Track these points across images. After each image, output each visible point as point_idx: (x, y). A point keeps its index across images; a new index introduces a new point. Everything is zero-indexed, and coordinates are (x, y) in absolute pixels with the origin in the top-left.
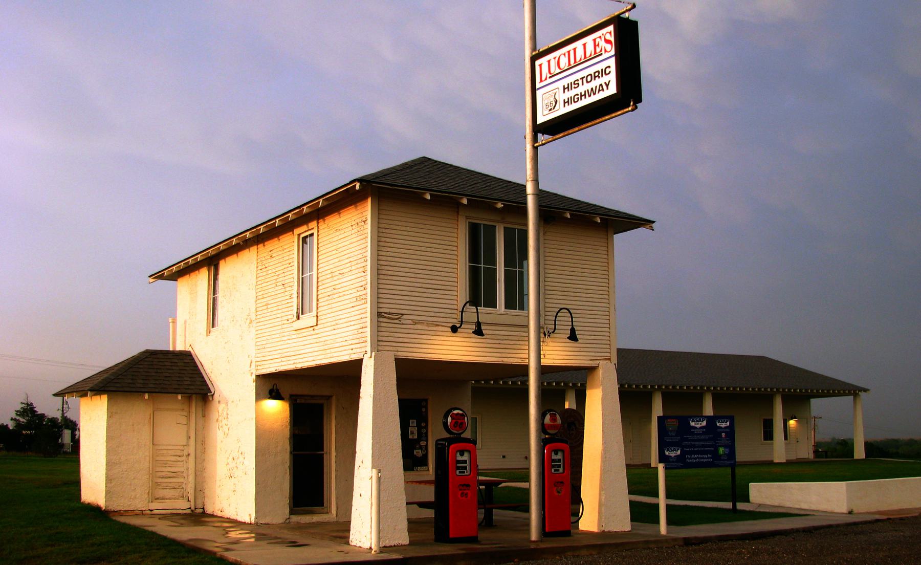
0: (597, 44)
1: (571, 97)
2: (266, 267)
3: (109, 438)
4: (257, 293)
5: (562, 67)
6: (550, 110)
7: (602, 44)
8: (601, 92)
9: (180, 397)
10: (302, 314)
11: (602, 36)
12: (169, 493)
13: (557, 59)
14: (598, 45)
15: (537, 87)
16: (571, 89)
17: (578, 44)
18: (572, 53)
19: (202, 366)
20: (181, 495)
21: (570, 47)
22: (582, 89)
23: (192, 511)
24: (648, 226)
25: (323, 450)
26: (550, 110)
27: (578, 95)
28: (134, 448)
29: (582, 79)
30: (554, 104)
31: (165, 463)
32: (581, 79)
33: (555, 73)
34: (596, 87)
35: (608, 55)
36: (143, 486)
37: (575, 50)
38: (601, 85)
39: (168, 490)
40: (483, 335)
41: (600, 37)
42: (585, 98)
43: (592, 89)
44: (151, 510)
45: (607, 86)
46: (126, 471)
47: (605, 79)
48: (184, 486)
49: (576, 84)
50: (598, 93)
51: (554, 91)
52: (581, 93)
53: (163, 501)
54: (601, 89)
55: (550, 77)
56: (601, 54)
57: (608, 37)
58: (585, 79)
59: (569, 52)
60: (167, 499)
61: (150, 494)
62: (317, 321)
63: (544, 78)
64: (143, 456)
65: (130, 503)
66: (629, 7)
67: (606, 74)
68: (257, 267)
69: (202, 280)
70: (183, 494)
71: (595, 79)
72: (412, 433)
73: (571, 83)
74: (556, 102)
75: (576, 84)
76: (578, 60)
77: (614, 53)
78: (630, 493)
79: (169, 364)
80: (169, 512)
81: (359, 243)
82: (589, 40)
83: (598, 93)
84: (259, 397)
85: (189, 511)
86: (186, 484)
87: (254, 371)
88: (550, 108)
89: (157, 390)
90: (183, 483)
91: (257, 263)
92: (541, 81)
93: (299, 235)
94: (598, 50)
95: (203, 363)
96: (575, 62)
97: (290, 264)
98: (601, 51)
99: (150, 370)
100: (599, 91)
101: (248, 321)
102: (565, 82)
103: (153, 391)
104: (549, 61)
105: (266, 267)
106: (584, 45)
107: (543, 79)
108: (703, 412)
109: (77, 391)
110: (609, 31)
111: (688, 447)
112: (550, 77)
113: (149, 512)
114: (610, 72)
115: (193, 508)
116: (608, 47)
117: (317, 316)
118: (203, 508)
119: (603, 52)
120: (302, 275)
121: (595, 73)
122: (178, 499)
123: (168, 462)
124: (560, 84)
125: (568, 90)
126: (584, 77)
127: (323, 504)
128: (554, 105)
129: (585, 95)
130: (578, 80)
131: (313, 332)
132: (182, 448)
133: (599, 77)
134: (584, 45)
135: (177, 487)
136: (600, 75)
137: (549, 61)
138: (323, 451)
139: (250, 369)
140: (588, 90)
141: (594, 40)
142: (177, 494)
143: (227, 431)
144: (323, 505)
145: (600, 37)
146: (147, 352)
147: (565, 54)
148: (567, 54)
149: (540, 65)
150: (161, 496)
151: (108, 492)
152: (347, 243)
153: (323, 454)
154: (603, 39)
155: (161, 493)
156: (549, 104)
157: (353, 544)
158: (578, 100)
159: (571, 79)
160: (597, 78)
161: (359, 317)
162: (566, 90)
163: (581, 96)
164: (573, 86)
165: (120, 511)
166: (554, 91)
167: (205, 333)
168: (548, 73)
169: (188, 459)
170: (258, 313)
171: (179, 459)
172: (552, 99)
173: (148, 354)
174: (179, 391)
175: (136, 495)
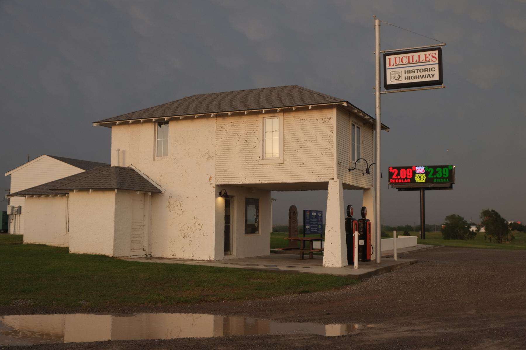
3: (116, 216)
4: (216, 142)
6: (396, 80)
7: (430, 57)
8: (429, 78)
9: (138, 193)
11: (430, 54)
13: (401, 58)
14: (428, 57)
16: (410, 73)
17: (416, 55)
19: (148, 177)
22: (416, 74)
24: (387, 130)
25: (229, 223)
26: (396, 80)
29: (417, 70)
30: (398, 77)
32: (416, 70)
33: (399, 64)
40: (369, 173)
41: (429, 54)
42: (419, 78)
43: (423, 76)
44: (131, 256)
45: (433, 76)
47: (432, 73)
48: (141, 242)
49: (413, 71)
51: (399, 72)
53: (134, 251)
54: (429, 76)
56: (430, 62)
57: (434, 55)
58: (419, 71)
60: (136, 250)
63: (392, 64)
66: (444, 44)
71: (425, 72)
74: (400, 77)
75: (413, 71)
78: (271, 248)
82: (422, 54)
84: (216, 197)
85: (145, 256)
88: (395, 79)
92: (390, 65)
94: (427, 59)
95: (148, 175)
98: (430, 60)
100: (428, 77)
102: (407, 69)
111: (313, 224)
112: (396, 65)
113: (130, 257)
114: (434, 70)
116: (434, 60)
117: (284, 159)
119: (431, 61)
120: (157, 139)
121: (425, 69)
123: (136, 229)
124: (403, 70)
127: (229, 250)
131: (279, 166)
133: (428, 71)
134: (419, 56)
136: (429, 70)
139: (209, 181)
141: (426, 55)
144: (229, 251)
145: (429, 54)
147: (406, 57)
148: (407, 57)
149: (390, 59)
151: (115, 246)
153: (230, 225)
154: (431, 55)
157: (327, 265)
158: (412, 77)
159: (411, 69)
160: (426, 72)
164: (411, 72)
165: (119, 257)
166: (400, 72)
170: (217, 153)
171: (140, 227)
172: (397, 75)
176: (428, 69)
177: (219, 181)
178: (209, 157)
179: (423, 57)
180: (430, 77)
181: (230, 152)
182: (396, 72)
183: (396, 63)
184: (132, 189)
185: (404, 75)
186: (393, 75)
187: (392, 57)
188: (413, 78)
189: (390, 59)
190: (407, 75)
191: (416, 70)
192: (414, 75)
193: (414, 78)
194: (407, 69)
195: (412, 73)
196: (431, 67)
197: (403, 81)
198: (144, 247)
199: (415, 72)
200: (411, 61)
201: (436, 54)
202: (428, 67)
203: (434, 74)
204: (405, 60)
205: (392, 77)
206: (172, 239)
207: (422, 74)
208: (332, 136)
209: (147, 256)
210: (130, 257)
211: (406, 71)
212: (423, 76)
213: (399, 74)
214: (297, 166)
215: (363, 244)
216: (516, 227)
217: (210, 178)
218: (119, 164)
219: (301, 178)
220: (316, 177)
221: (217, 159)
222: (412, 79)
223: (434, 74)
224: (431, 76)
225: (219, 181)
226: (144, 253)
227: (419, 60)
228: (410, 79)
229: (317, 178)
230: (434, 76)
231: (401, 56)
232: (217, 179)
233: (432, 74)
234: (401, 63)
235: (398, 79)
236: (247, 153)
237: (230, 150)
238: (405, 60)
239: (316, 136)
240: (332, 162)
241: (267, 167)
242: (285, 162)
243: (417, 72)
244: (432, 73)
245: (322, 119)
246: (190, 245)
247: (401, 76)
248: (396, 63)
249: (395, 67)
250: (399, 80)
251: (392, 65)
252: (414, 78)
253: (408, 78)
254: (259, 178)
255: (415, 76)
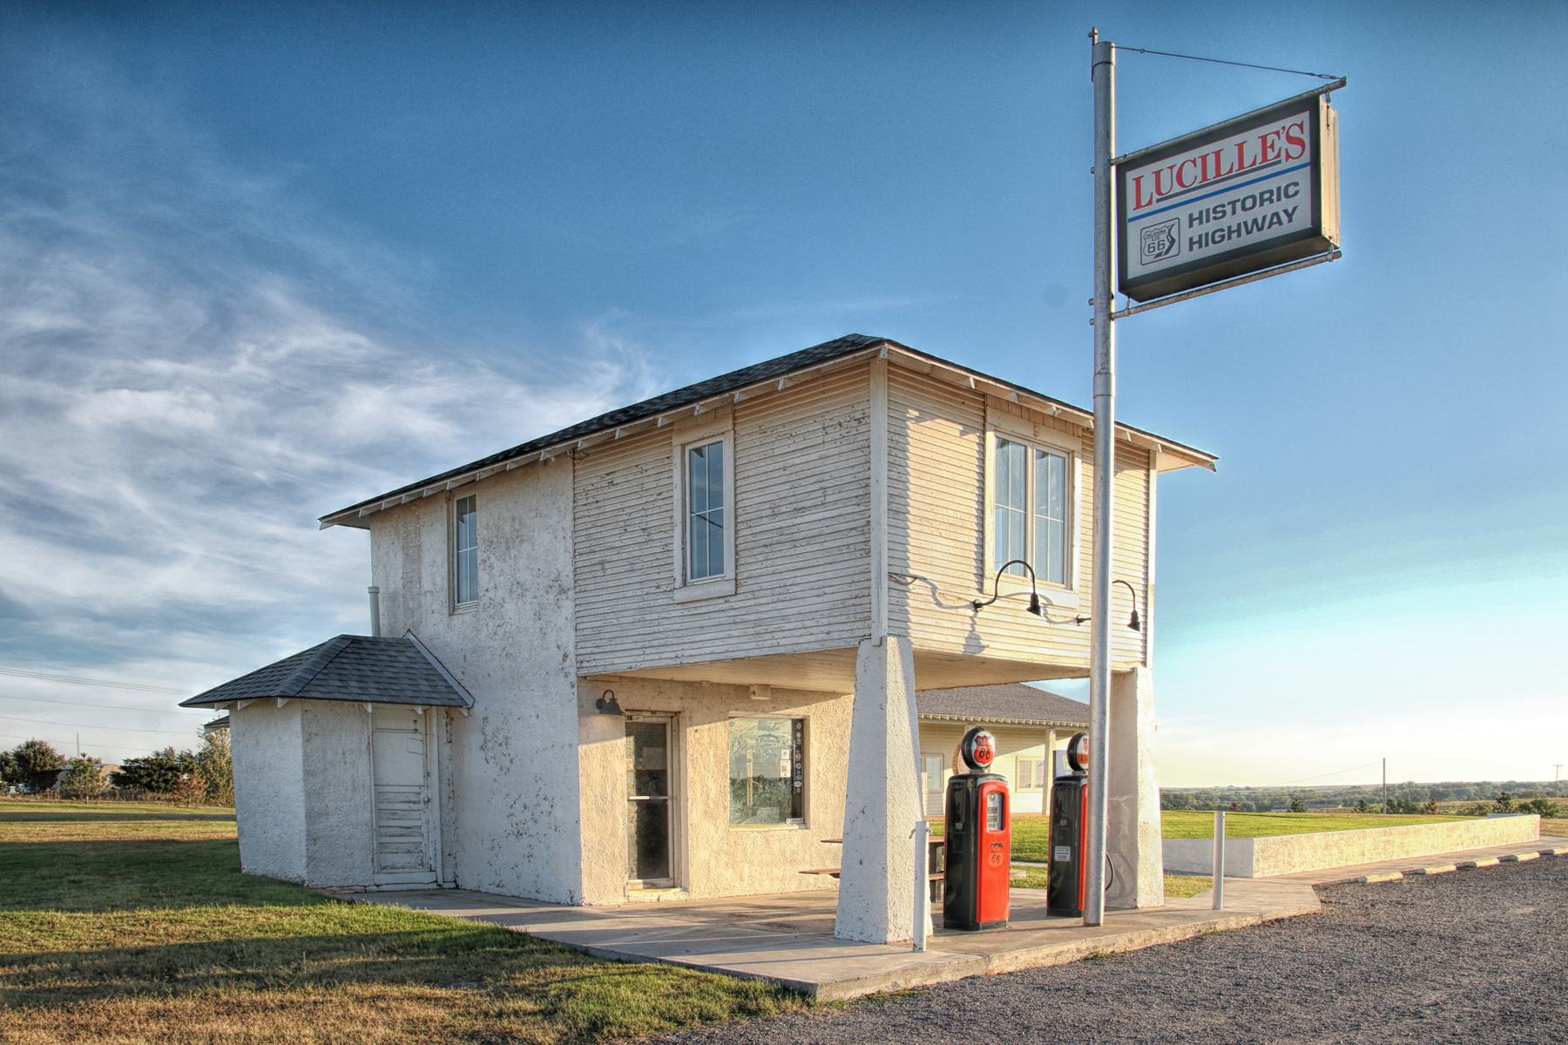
0: (1269, 144)
1: (1207, 234)
2: (597, 502)
5: (1163, 191)
7: (1282, 143)
10: (459, 602)
11: (1282, 131)
12: (400, 859)
13: (1175, 170)
14: (1272, 146)
15: (1129, 217)
16: (1208, 221)
17: (1228, 146)
18: (1211, 160)
20: (420, 862)
21: (1209, 149)
22: (1230, 221)
23: (439, 885)
27: (1222, 230)
28: (346, 790)
29: (1233, 203)
30: (1167, 245)
31: (394, 812)
32: (1229, 204)
34: (1264, 218)
35: (1292, 163)
36: (364, 848)
37: (1217, 154)
38: (1277, 214)
39: (400, 855)
41: (1277, 133)
42: (1239, 235)
43: (1255, 221)
44: (378, 886)
45: (1290, 216)
46: (337, 826)
47: (1287, 204)
49: (1218, 212)
50: (1269, 227)
51: (1172, 223)
52: (1229, 228)
54: (1275, 220)
55: (1158, 201)
56: (1280, 162)
57: (1295, 132)
58: (1239, 205)
59: (1204, 158)
60: (398, 868)
61: (375, 860)
62: (736, 588)
63: (1144, 201)
64: (362, 802)
65: (346, 875)
67: (1287, 196)
68: (574, 502)
69: (432, 525)
70: (422, 860)
71: (1261, 205)
72: (785, 770)
73: (1208, 210)
74: (1172, 242)
76: (1224, 170)
77: (1308, 160)
79: (387, 658)
80: (404, 887)
81: (851, 455)
82: (1251, 139)
83: (1269, 227)
85: (434, 886)
86: (425, 845)
87: (573, 670)
88: (1157, 252)
89: (385, 699)
90: (421, 843)
91: (575, 495)
92: (1139, 206)
93: (683, 446)
94: (1271, 155)
96: (1218, 173)
97: (660, 494)
98: (1278, 155)
99: (362, 667)
101: (555, 590)
102: (1194, 209)
103: (379, 699)
104: (1158, 174)
105: (597, 502)
106: (1240, 146)
107: (1144, 202)
108: (633, 743)
109: (242, 699)
110: (1299, 123)
112: (1158, 201)
115: (440, 881)
116: (1295, 150)
117: (736, 580)
118: (455, 881)
120: (458, 550)
121: (1262, 194)
122: (415, 868)
124: (1183, 213)
125: (1201, 223)
126: (1238, 200)
127: (668, 873)
128: (1166, 247)
129: (1239, 231)
130: (1223, 206)
132: (416, 790)
133: (1272, 202)
134: (1240, 146)
135: (413, 849)
136: (1275, 197)
137: (1158, 174)
138: (666, 794)
140: (1245, 223)
141: (1264, 138)
142: (413, 861)
143: (507, 764)
145: (1277, 133)
146: (344, 638)
147: (1194, 162)
148: (1199, 162)
149: (1138, 180)
150: (390, 863)
152: (813, 457)
153: (666, 800)
154: (1283, 136)
155: (390, 859)
156: (1156, 246)
159: (1210, 203)
161: (849, 580)
162: (1196, 223)
163: (1230, 232)
164: (1212, 215)
166: (1172, 223)
167: (445, 611)
168: (1155, 194)
169: (427, 808)
170: (577, 578)
172: (1163, 237)
173: (348, 642)
174: (418, 701)
175: (354, 863)
176: (1271, 192)
177: (585, 664)
178: (560, 593)
179: (1253, 150)
180: (1280, 222)
181: (609, 572)
182: (1159, 227)
183: (1158, 191)
184: (321, 696)
185: (1188, 233)
186: (1149, 241)
187: (1146, 172)
188: (1217, 239)
189: (1138, 180)
190: (1198, 230)
191: (1229, 204)
192: (1214, 221)
193: (1223, 237)
194: (1194, 209)
195: (1215, 218)
196: (1282, 181)
197: (1184, 255)
198: (432, 862)
199: (1224, 213)
200: (1211, 174)
201: (1301, 126)
202: (1272, 184)
203: (1295, 209)
204: (1191, 174)
205: (1147, 246)
206: (493, 840)
207: (1249, 217)
208: (867, 481)
209: (439, 885)
210: (375, 888)
211: (1196, 215)
212: (1255, 221)
213: (1170, 230)
214: (770, 600)
215: (1068, 858)
216: (11, 779)
217: (566, 656)
218: (379, 634)
219: (783, 642)
220: (822, 632)
221: (582, 595)
222: (1214, 242)
223: (1295, 209)
224: (1284, 218)
225: (585, 664)
226: (430, 877)
227: (1241, 166)
228: (1207, 245)
229: (825, 636)
230: (1294, 217)
231: (1177, 160)
232: (579, 658)
233: (1286, 211)
234: (1177, 188)
235: (1166, 253)
236: (646, 571)
237: (607, 566)
238: (1191, 174)
239: (822, 488)
240: (866, 576)
241: (695, 612)
242: (740, 591)
243: (1234, 212)
244: (1287, 204)
245: (840, 424)
246: (531, 859)
247: (1176, 237)
248: (1158, 191)
249: (1155, 206)
250: (1170, 254)
251: (1147, 200)
252: (1223, 237)
253: (1200, 242)
254: (675, 648)
255: (1226, 229)
